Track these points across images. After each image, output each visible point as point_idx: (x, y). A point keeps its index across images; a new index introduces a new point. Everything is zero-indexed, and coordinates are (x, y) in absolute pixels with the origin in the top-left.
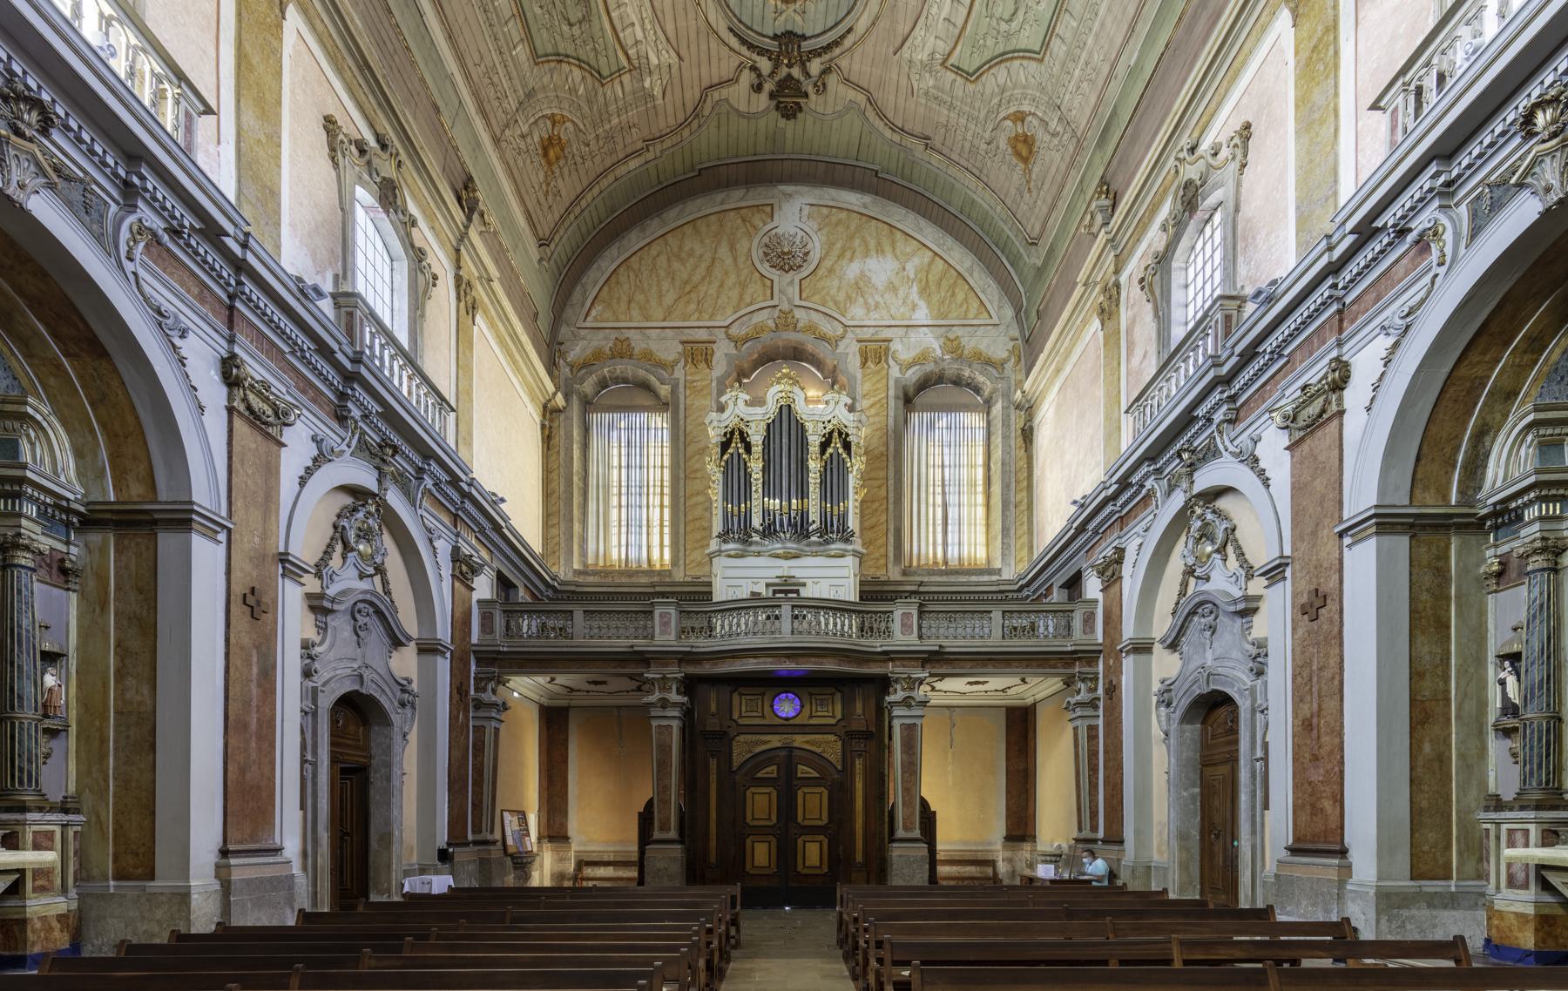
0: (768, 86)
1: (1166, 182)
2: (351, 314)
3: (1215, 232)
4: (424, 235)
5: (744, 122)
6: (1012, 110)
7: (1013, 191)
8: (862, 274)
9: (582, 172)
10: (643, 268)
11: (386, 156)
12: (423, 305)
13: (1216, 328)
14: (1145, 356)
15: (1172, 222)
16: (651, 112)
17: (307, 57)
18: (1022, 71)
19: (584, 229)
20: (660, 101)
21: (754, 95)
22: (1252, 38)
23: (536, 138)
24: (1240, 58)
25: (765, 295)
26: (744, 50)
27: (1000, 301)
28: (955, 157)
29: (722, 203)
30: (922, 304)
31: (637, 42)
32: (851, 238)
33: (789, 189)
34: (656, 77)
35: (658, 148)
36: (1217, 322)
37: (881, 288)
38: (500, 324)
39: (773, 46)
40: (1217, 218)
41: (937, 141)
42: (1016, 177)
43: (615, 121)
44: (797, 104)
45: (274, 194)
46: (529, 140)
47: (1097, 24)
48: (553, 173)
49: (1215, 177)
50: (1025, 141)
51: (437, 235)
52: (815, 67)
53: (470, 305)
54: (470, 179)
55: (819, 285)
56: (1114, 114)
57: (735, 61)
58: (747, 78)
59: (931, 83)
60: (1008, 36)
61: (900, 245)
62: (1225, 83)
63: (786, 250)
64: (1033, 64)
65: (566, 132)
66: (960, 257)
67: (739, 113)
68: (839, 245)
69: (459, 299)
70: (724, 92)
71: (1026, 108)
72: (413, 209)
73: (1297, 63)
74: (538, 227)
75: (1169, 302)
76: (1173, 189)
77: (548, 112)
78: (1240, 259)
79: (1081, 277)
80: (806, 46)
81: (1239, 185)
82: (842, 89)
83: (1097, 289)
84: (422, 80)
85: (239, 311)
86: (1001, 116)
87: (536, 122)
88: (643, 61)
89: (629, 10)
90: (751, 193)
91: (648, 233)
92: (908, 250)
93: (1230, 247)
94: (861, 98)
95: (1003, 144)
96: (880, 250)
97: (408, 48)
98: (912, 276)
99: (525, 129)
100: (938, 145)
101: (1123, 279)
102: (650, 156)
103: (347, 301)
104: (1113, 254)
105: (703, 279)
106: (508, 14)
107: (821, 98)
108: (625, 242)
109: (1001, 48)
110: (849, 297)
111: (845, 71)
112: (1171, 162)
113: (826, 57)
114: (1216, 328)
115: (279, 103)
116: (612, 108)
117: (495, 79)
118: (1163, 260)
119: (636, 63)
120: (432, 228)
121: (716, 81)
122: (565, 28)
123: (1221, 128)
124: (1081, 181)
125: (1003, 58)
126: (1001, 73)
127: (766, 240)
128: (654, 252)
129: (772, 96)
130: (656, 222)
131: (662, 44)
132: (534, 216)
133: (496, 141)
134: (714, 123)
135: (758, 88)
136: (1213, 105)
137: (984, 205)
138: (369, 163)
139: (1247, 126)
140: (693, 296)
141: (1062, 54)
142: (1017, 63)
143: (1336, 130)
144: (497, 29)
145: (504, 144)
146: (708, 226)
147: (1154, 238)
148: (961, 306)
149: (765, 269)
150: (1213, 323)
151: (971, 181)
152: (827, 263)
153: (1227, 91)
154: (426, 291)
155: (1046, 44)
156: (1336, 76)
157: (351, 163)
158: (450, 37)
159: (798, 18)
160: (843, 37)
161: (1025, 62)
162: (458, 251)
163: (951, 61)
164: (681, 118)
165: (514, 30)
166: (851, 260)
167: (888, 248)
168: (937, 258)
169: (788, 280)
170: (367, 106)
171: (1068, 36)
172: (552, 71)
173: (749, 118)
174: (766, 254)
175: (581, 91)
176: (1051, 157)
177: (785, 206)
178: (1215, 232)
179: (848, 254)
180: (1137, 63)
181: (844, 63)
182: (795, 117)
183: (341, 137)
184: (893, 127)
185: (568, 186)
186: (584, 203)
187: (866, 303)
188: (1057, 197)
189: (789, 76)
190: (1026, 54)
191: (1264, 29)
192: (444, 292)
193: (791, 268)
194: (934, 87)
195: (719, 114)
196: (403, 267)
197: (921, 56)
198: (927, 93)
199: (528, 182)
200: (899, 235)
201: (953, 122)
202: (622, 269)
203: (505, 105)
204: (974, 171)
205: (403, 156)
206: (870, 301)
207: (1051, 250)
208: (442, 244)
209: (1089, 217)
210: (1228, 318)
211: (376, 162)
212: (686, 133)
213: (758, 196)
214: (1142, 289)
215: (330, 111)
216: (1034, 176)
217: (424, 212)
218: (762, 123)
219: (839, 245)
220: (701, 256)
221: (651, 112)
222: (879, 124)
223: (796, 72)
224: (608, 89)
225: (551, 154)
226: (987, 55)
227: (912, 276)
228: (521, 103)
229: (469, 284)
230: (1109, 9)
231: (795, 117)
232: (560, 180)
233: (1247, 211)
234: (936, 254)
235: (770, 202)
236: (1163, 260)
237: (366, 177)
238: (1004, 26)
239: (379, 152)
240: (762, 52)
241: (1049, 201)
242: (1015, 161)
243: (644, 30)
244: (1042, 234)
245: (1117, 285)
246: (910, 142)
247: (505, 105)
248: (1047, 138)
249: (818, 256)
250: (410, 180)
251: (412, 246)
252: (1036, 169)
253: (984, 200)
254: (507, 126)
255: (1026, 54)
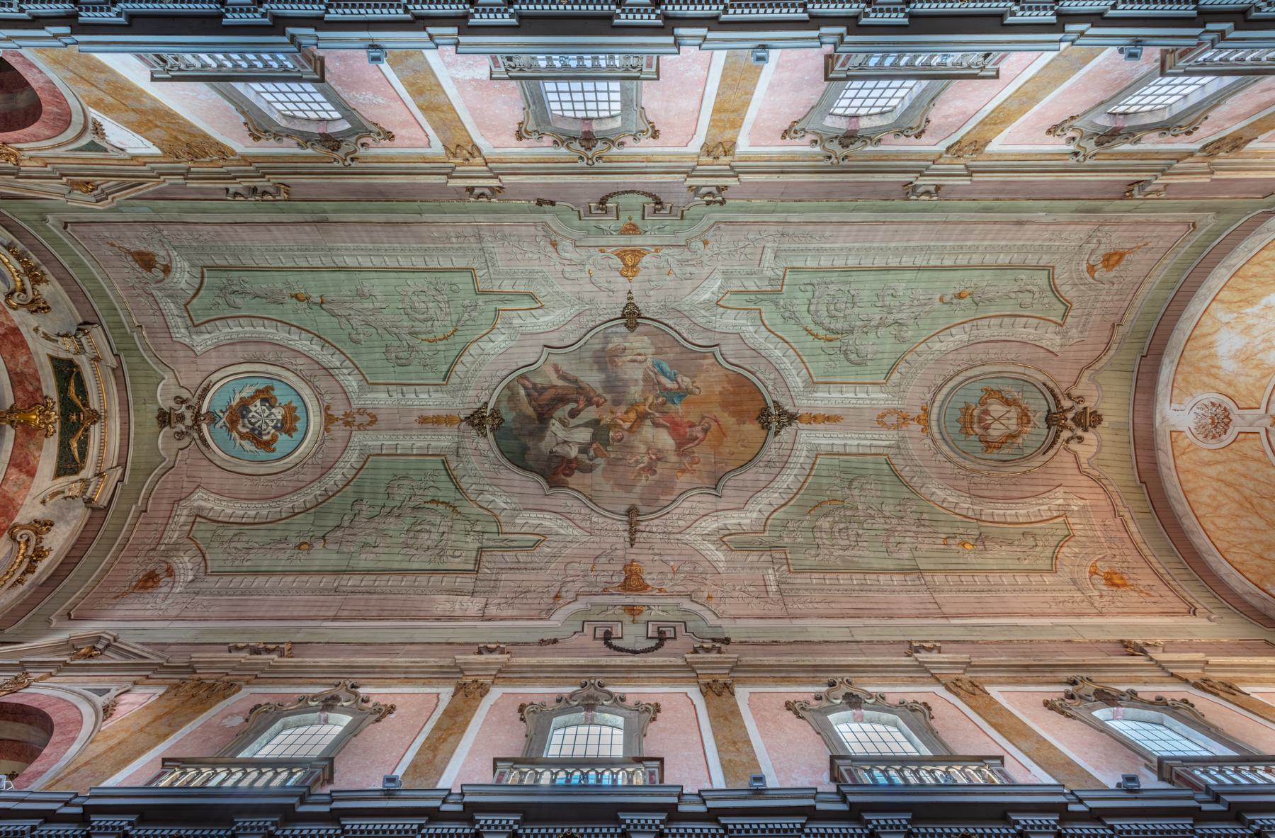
0: (1079, 432)
1: (1106, 157)
2: (1178, 776)
3: (1132, 103)
4: (1147, 691)
5: (1104, 449)
6: (1087, 275)
7: (1149, 256)
8: (1234, 357)
9: (1135, 565)
10: (1227, 539)
11: (1081, 685)
12: (1206, 722)
13: (1193, 58)
14: (1268, 90)
15: (1131, 139)
16: (1094, 509)
17: (1012, 695)
18: (1061, 277)
19: (1186, 577)
20: (1088, 502)
21: (1085, 442)
22: (1006, 158)
23: (1105, 588)
24: (1018, 158)
25: (1254, 439)
26: (1056, 447)
27: (1262, 233)
28: (1126, 304)
29: (1169, 469)
30: (1264, 301)
31: (1049, 510)
32: (1199, 370)
33: (1158, 419)
34: (1071, 502)
35: (1121, 508)
36: (1187, 62)
37: (1247, 340)
38: (1261, 675)
39: (1054, 429)
40: (1121, 109)
41: (1115, 319)
42: (1137, 257)
43: (1099, 534)
44: (1091, 414)
45: (1070, 763)
46: (1104, 593)
47: (1029, 243)
48: (1132, 585)
49: (1090, 130)
50: (1108, 260)
51: (1152, 683)
52: (1067, 404)
53: (1227, 689)
54: (1122, 641)
55: (1244, 393)
56: (1077, 211)
57: (1063, 452)
58: (1074, 446)
59: (1074, 330)
60: (1042, 291)
61: (1205, 330)
62: (1034, 158)
63: (1210, 421)
64: (1057, 271)
65: (1103, 567)
66: (1220, 276)
67: (1098, 452)
68: (1206, 379)
69: (1216, 695)
70: (1083, 460)
71: (1084, 267)
72: (1123, 688)
73: (1005, 128)
74: (1176, 610)
75: (1201, 103)
76: (1108, 151)
77: (1087, 575)
78: (1136, 77)
79: (1205, 179)
80: (1054, 409)
81: (1085, 113)
82: (1081, 386)
83: (1216, 161)
84: (1050, 641)
85: (208, 407)
86: (1092, 281)
87: (1093, 585)
88: (1061, 508)
89: (1031, 510)
90: (1162, 447)
91: (1195, 529)
92: (1210, 322)
93: (1130, 90)
94: (1087, 373)
95: (1112, 274)
96: (1210, 345)
97: (1031, 641)
98: (1235, 315)
99: (1096, 593)
100: (1119, 317)
101: (1197, 146)
102: (1127, 515)
103: (1163, 767)
104: (1177, 165)
105: (1238, 491)
106: (1026, 579)
107: (1086, 399)
108: (1203, 549)
109: (1050, 294)
110: (1257, 366)
111: (1069, 385)
112: (1088, 162)
113: (1060, 397)
114: (1193, 58)
115: (1024, 724)
116: (1090, 533)
117: (1061, 599)
118: (1164, 128)
119: (1062, 513)
120: (1145, 683)
121: (1075, 465)
122: (1038, 549)
123: (1058, 145)
124: (1129, 212)
125: (1055, 290)
126: (1063, 289)
127: (1200, 437)
128: (1211, 527)
129: (1086, 430)
130: (1184, 520)
131: (1051, 495)
132: (1165, 610)
133: (1101, 614)
134: (1105, 469)
135: (1080, 439)
136: (1048, 157)
137: (1164, 272)
138: (1081, 697)
139: (1049, 132)
140: (1255, 501)
141: (1048, 256)
142: (1056, 281)
143: (1026, 82)
144: (1033, 588)
145: (1104, 610)
146: (1188, 481)
147: (1150, 143)
148: (1267, 266)
149: (1227, 438)
150: (1192, 63)
151: (1145, 289)
152: (1222, 387)
153: (1036, 154)
154: (1195, 715)
155: (1043, 268)
156: (1002, 103)
157: (1076, 707)
158: (1032, 615)
159: (1038, 415)
160: (1048, 388)
161: (1056, 276)
162: (1172, 675)
163: (1060, 321)
164: (1100, 490)
165: (1035, 578)
166: (1219, 368)
167: (1209, 339)
168: (1218, 297)
169: (1238, 418)
170: (1049, 679)
171: (1037, 257)
172: (1062, 564)
173: (1102, 446)
174: (1214, 437)
175: (1077, 550)
176: (1116, 238)
177: (1172, 422)
178: (1132, 103)
179: (1213, 371)
180: (1041, 211)
181: (1064, 386)
182: (1100, 416)
183: (1057, 703)
184: (1107, 349)
185: (1145, 578)
186: (1162, 571)
187: (1263, 350)
188: (1148, 223)
189: (1073, 419)
190: (1051, 278)
191: (999, 154)
192: (1203, 702)
193: (1227, 417)
194: (1077, 328)
195: (1098, 466)
196: (1168, 720)
197: (1058, 339)
198: (1081, 332)
199: (1137, 605)
200: (1196, 333)
201: (1100, 311)
202: (1228, 557)
203: (1078, 600)
204: (1135, 288)
205: (1085, 675)
206: (1260, 347)
207: (1196, 210)
208: (1161, 683)
209: (1149, 196)
210: (1182, 55)
211: (1082, 693)
212: (1111, 488)
213: (1163, 441)
214: (1196, 129)
215: (1041, 699)
216: (1134, 245)
217: (1131, 682)
218: (1104, 437)
219: (1206, 379)
220: (1215, 490)
221: (1094, 509)
222: (1105, 360)
223: (1070, 415)
224: (1077, 533)
225: (1118, 582)
226: (1054, 300)
227: (1235, 315)
228: (1079, 590)
229: (1205, 680)
230: (1020, 239)
231: (1100, 416)
232: (1139, 582)
233: (1100, 96)
234: (1213, 300)
235: (1168, 433)
236: (1164, 128)
237: (1089, 704)
238: (1037, 295)
239: (1076, 687)
240: (1057, 436)
241: (1152, 227)
242: (1124, 262)
243: (1043, 505)
244: (1183, 223)
245: (1204, 148)
246: (1117, 337)
247: (1078, 600)
248: (1103, 247)
249: (1215, 395)
250: (1104, 679)
251: (1151, 703)
252: (1129, 245)
253: (1159, 275)
254: (1092, 604)
255: (1051, 278)
